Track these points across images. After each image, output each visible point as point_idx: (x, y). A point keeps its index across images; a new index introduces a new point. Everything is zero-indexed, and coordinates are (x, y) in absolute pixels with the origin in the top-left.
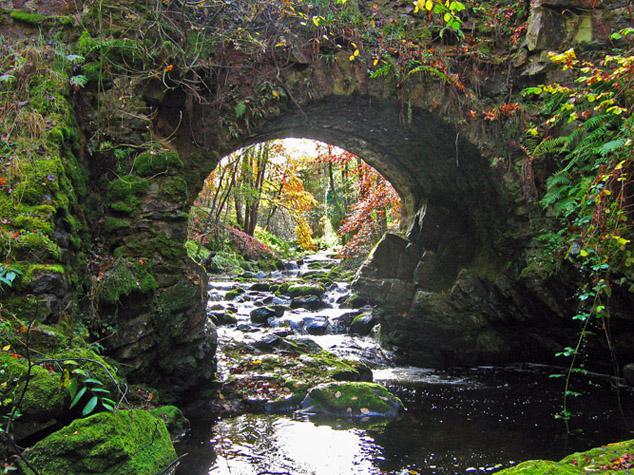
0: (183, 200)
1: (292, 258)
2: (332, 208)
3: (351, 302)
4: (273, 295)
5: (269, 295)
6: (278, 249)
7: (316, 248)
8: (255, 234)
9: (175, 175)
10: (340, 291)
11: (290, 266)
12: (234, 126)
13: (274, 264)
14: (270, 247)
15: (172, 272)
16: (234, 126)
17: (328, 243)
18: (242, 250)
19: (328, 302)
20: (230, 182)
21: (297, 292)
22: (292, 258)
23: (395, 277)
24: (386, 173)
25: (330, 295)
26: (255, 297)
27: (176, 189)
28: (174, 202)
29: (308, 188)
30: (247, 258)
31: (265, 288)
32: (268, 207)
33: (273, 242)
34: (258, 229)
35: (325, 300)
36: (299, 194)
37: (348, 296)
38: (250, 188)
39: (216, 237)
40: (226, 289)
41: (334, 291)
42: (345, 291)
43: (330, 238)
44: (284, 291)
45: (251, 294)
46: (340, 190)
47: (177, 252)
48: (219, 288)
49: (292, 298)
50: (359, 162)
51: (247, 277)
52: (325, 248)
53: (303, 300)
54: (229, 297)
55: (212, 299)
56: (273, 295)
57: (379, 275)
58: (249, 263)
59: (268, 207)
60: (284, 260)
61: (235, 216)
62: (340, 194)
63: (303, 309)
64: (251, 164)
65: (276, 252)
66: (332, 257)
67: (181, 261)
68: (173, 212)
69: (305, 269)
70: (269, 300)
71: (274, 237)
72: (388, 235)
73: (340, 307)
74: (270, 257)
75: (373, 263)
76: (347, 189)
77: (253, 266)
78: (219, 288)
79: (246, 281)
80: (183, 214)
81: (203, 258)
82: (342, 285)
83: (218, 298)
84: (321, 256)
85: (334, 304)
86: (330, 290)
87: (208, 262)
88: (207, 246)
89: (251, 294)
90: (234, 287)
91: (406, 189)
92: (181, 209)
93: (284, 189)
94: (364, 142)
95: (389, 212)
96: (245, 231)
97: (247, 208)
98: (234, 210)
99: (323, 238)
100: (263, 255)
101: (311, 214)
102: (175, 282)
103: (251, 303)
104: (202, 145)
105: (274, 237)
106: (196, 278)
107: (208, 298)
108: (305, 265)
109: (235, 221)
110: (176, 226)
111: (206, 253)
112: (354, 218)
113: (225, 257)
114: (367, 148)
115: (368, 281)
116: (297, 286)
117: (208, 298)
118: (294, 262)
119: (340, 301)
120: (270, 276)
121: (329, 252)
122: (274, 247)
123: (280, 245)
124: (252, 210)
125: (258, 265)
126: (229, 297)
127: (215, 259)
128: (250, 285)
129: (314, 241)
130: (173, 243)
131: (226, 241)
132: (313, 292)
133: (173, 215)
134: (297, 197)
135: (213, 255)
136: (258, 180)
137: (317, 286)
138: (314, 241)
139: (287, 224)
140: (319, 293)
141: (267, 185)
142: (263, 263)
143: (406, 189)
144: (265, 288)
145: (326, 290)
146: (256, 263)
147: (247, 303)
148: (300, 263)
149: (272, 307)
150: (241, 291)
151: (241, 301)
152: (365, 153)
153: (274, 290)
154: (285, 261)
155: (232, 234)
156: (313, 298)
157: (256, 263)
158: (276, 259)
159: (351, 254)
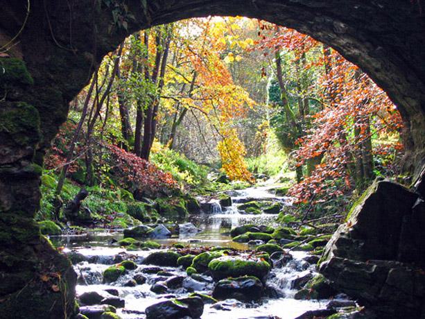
0: (33, 142)
1: (213, 194)
2: (279, 109)
3: (314, 288)
4: (184, 274)
5: (176, 273)
6: (189, 179)
7: (254, 176)
8: (151, 156)
9: (17, 99)
10: (297, 268)
11: (209, 209)
12: (121, 8)
13: (182, 205)
14: (177, 179)
15: (16, 267)
16: (121, 8)
17: (270, 167)
18: (130, 184)
19: (276, 286)
20: (111, 69)
21: (223, 271)
22: (213, 194)
23: (394, 257)
24: (378, 75)
25: (280, 274)
26: (155, 276)
27: (21, 125)
28: (17, 147)
29: (242, 81)
30: (138, 196)
31: (169, 260)
32: (173, 110)
33: (182, 167)
34: (156, 146)
35: (270, 283)
36: (225, 89)
37: (309, 277)
38: (143, 82)
39: (88, 162)
40: (106, 261)
41: (287, 268)
42: (305, 267)
43: (275, 159)
44: (202, 266)
45: (145, 271)
46: (293, 85)
47: (22, 234)
48: (94, 260)
49: (216, 279)
50: (327, 53)
51: (138, 236)
52: (266, 176)
53: (235, 284)
54: (110, 277)
55: (82, 282)
56: (184, 274)
57: (366, 255)
58: (141, 205)
59: (173, 110)
60: (199, 198)
61: (119, 124)
62: (293, 93)
63: (235, 301)
64: (146, 41)
65: (187, 186)
66: (281, 192)
67: (28, 249)
68: (17, 163)
69: (235, 216)
70: (177, 283)
71: (182, 158)
72: (383, 186)
73: (297, 297)
74: (176, 193)
75: (357, 232)
76: (305, 82)
77: (148, 208)
78: (94, 260)
79: (138, 246)
80: (32, 166)
81: (66, 200)
82: (299, 256)
83: (91, 280)
84: (259, 192)
85: (288, 291)
86: (280, 266)
87: (75, 206)
88: (75, 179)
89: (145, 271)
90: (118, 259)
91: (414, 103)
92: (29, 158)
93: (199, 79)
94: (342, 25)
95: (376, 121)
96: (135, 151)
97: (139, 113)
98: (117, 112)
99: (262, 157)
100: (165, 191)
101: (244, 124)
102: (20, 285)
103: (146, 288)
104: (65, 43)
105: (182, 158)
106: (55, 280)
107: (73, 279)
108: (234, 207)
109: (119, 134)
110: (19, 188)
111: (72, 191)
112: (317, 136)
113: (103, 196)
114: (346, 34)
115: (347, 264)
116: (226, 258)
117: (73, 279)
118: (215, 202)
119: (297, 284)
120: (176, 231)
121: (273, 183)
122: (182, 175)
123: (192, 172)
124: (148, 118)
125: (157, 207)
126: (110, 277)
127: (87, 201)
128: (145, 254)
129: (248, 164)
130: (16, 218)
131: (104, 168)
132: (251, 270)
133: (15, 170)
134: (221, 94)
135: (82, 196)
136: (156, 69)
137: (258, 260)
138: (248, 164)
139: (203, 135)
140: (261, 273)
141: (172, 75)
142: (164, 203)
143: (414, 103)
144: (169, 260)
145: (272, 266)
146: (152, 203)
147: (140, 288)
148: (226, 203)
149: (183, 301)
150: (130, 266)
151: (130, 284)
152: (343, 41)
153: (185, 264)
154: (200, 199)
155: (115, 156)
156: (251, 281)
157: (152, 203)
158: (186, 197)
159: (312, 197)
